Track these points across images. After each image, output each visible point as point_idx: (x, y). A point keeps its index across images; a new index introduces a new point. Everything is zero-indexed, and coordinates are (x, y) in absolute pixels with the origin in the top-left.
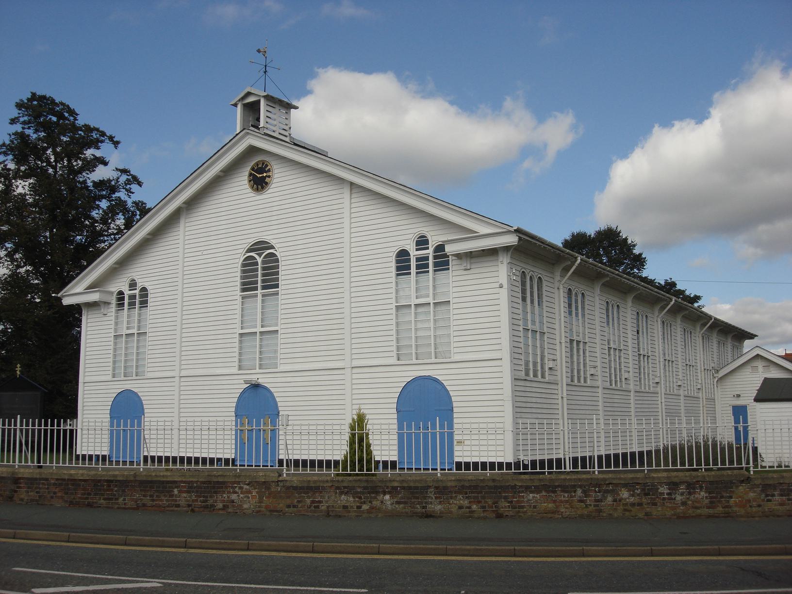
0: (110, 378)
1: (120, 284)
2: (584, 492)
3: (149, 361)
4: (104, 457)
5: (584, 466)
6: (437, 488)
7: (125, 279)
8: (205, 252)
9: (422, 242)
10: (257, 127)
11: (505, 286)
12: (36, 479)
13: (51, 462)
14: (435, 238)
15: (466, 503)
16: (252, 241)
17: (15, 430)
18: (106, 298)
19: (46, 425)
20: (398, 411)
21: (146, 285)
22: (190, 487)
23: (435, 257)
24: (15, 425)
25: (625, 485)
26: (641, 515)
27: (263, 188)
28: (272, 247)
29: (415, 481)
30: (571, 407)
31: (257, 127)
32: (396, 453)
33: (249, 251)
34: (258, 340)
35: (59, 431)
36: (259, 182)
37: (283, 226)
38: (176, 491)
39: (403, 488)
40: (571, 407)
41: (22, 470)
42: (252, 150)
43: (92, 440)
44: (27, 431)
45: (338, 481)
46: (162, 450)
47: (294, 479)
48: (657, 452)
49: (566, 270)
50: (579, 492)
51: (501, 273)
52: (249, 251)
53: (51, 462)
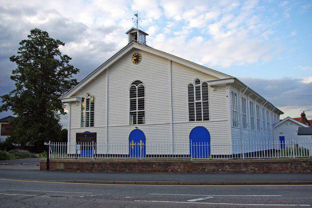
0: (80, 127)
1: (84, 95)
2: (291, 164)
5: (239, 157)
6: (244, 163)
9: (198, 81)
10: (136, 42)
11: (229, 96)
12: (101, 163)
13: (277, 156)
15: (253, 168)
17: (92, 147)
18: (79, 100)
22: (159, 164)
23: (202, 87)
24: (92, 144)
25: (304, 162)
26: (288, 172)
28: (141, 83)
31: (136, 42)
33: (133, 84)
36: (137, 60)
38: (154, 166)
39: (232, 163)
41: (80, 160)
42: (134, 49)
47: (196, 161)
48: (269, 150)
49: (242, 92)
50: (289, 164)
51: (228, 91)
52: (133, 84)
53: (277, 156)
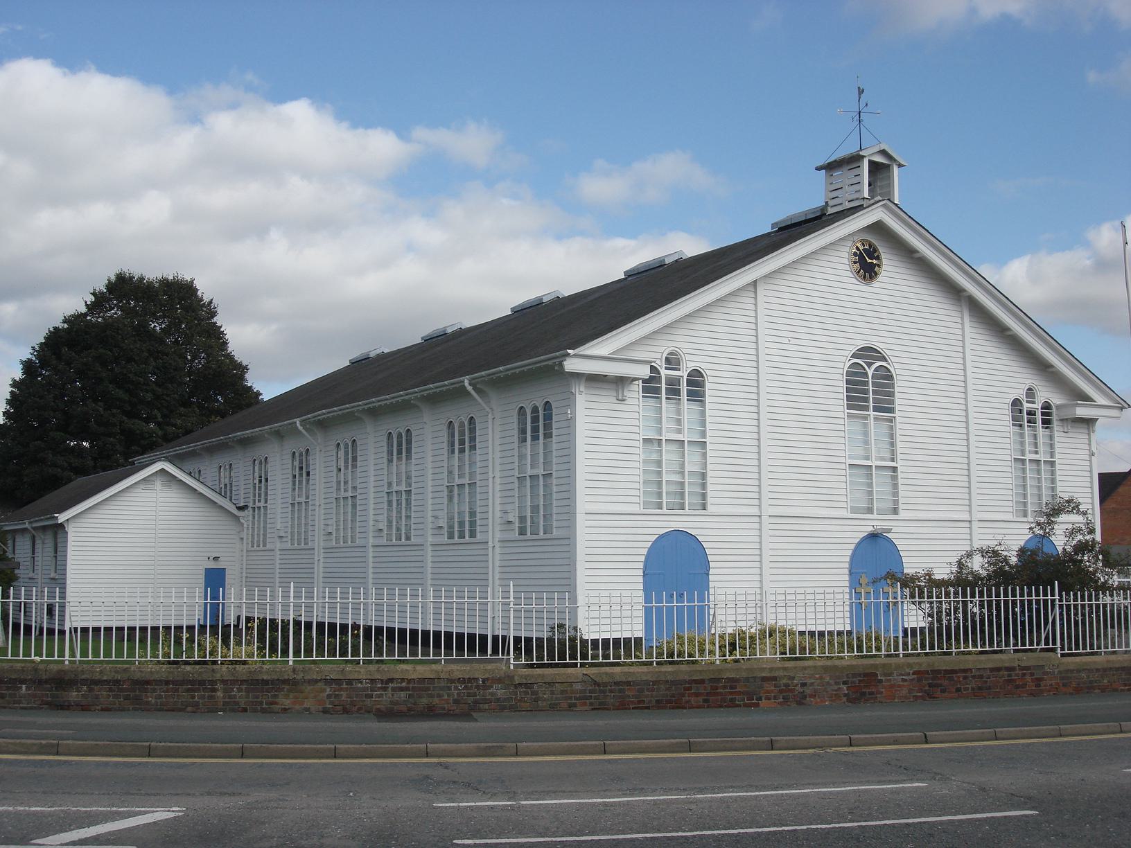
3: (636, 479)
4: (638, 641)
7: (662, 349)
8: (793, 341)
9: (1030, 393)
13: (1007, 644)
14: (1043, 394)
16: (862, 344)
19: (1030, 594)
20: (851, 573)
21: (702, 366)
24: (1053, 595)
27: (871, 278)
29: (771, 669)
30: (483, 558)
32: (641, 627)
33: (854, 356)
34: (878, 477)
35: (1098, 606)
36: (867, 267)
37: (850, 323)
40: (483, 558)
43: (828, 615)
44: (990, 603)
45: (785, 669)
46: (608, 628)
